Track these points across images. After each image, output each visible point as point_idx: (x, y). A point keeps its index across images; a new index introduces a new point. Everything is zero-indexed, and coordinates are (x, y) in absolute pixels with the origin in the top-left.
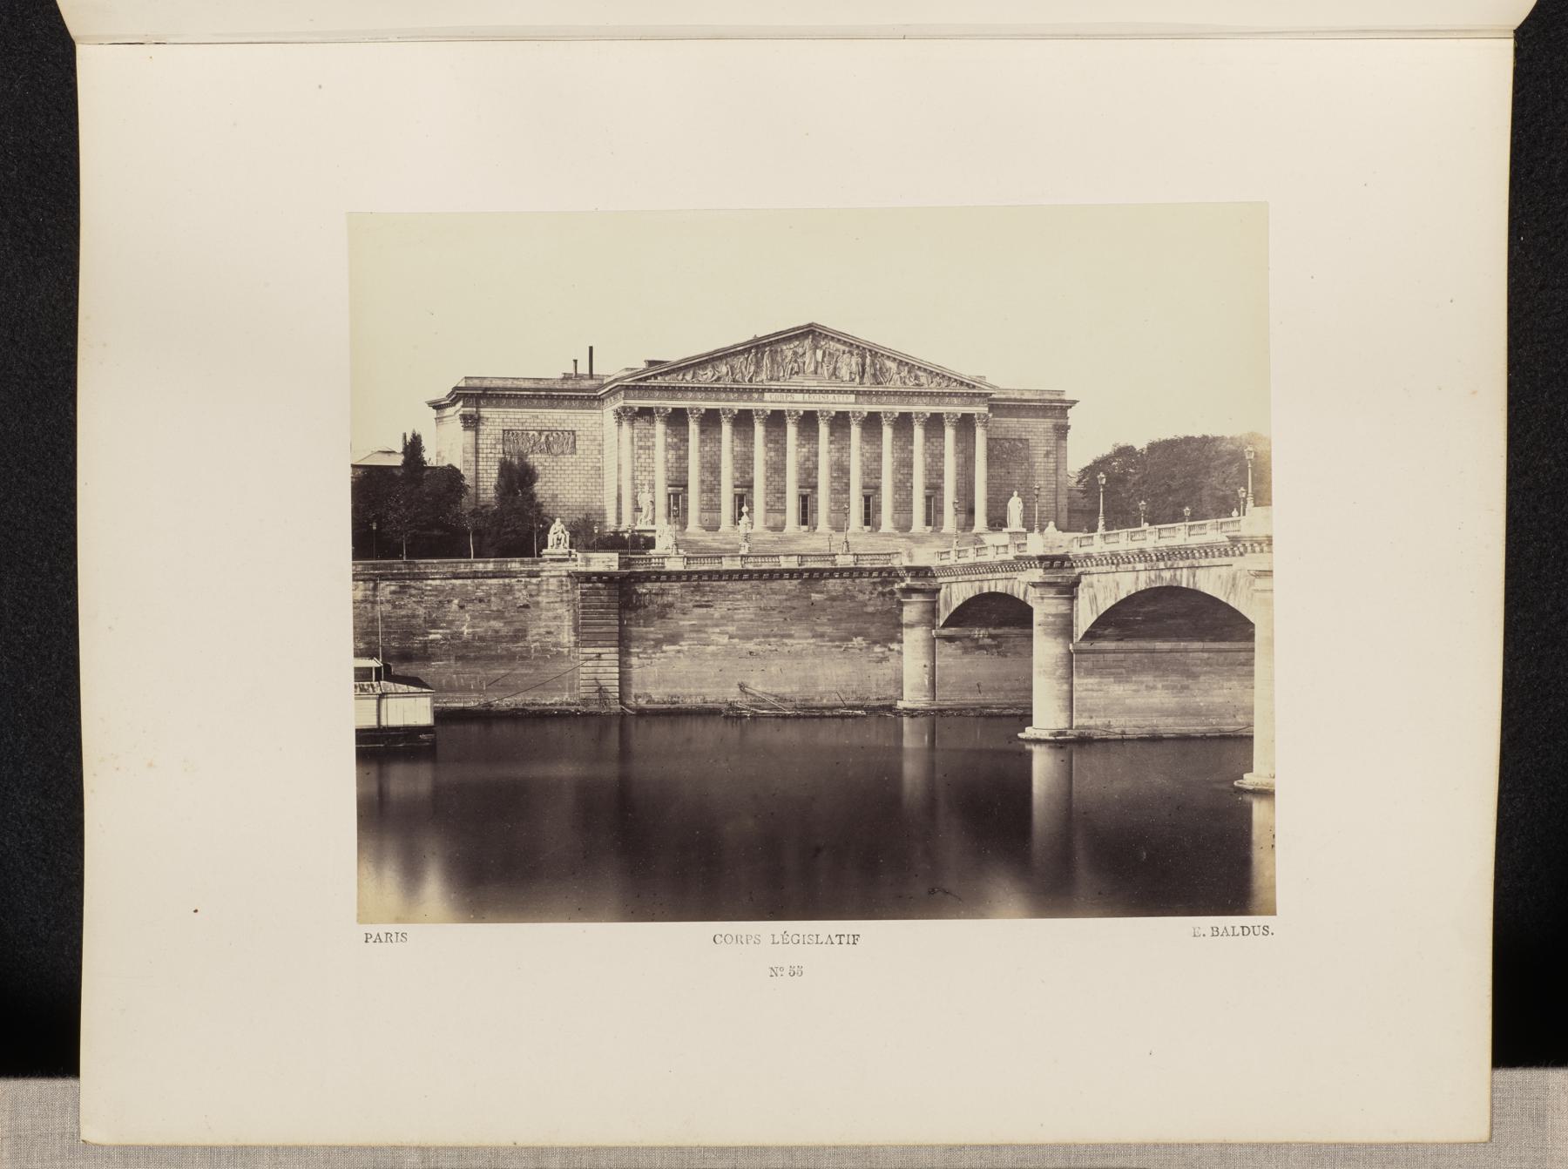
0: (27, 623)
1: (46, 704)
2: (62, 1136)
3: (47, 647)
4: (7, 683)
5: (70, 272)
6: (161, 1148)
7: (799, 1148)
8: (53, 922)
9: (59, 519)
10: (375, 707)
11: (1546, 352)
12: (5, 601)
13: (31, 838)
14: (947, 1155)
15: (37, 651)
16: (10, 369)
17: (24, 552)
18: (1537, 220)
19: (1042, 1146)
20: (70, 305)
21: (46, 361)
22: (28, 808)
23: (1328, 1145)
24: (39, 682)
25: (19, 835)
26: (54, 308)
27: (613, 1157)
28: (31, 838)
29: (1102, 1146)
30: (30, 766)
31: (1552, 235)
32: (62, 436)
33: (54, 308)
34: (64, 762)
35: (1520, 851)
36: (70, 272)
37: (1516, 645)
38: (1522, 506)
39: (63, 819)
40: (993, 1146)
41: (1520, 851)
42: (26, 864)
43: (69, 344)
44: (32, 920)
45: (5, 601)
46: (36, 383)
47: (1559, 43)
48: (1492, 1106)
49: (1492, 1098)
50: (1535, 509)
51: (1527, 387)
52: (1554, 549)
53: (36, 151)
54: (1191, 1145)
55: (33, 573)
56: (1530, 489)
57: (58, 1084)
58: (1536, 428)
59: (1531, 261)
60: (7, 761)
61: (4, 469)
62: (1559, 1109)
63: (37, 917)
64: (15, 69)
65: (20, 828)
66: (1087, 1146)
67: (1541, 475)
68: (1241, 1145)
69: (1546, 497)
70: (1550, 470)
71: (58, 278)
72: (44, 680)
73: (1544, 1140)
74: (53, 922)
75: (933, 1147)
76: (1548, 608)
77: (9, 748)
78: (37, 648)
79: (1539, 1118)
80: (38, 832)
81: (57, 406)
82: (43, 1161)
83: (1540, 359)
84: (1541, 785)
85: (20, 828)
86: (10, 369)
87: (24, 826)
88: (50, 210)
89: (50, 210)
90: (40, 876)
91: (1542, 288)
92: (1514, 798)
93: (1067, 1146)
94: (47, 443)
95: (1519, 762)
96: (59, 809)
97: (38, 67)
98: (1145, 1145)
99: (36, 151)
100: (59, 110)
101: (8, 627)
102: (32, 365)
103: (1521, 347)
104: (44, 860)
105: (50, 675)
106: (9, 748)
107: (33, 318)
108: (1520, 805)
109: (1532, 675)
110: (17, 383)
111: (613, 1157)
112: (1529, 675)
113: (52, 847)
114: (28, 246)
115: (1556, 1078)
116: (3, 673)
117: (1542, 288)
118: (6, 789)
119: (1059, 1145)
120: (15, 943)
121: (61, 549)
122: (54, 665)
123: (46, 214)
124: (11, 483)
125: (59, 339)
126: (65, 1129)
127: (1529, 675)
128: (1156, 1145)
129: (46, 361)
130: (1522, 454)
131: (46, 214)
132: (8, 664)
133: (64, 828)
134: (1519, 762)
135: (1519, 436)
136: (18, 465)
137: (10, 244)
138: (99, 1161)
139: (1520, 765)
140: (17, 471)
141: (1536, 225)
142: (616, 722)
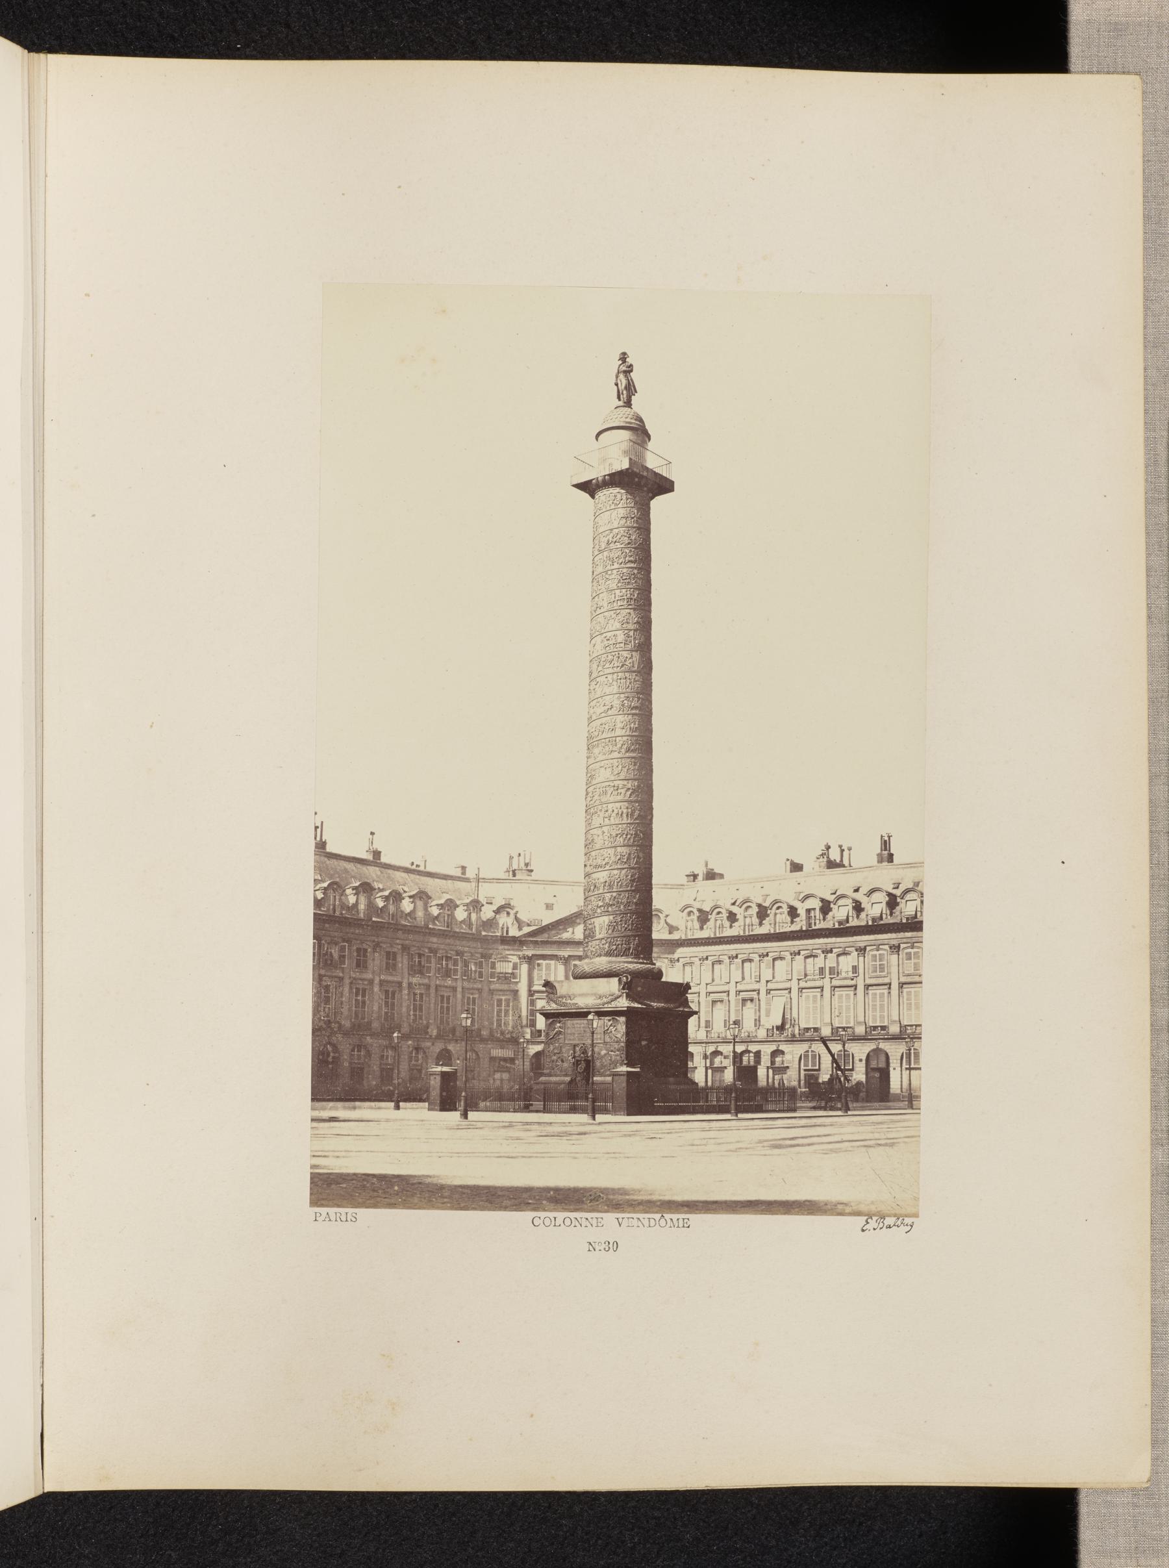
0: (623, 1542)
3: (648, 1521)
9: (519, 1510)
11: (352, 22)
12: (602, 1563)
13: (838, 1537)
15: (652, 1532)
17: (553, 1544)
20: (305, 1498)
22: (809, 1541)
23: (1145, 240)
30: (766, 1538)
31: (235, 15)
32: (436, 1506)
34: (762, 1503)
35: (852, 48)
39: (819, 1506)
41: (852, 48)
42: (864, 1542)
44: (920, 1536)
45: (602, 1563)
46: (383, 1532)
50: (509, 33)
51: (387, 41)
52: (549, 13)
54: (1146, 377)
55: (573, 1535)
56: (489, 38)
59: (261, 37)
60: (761, 1561)
61: (470, 1565)
64: (69, 1554)
66: (1146, 480)
68: (1145, 327)
70: (470, 18)
71: (279, 1510)
73: (1140, 24)
76: (608, 20)
77: (748, 1559)
79: (1118, 29)
80: (832, 1530)
82: (1161, 1525)
83: (359, 28)
84: (785, 27)
87: (826, 1544)
88: (210, 1518)
89: (210, 1518)
90: (877, 1528)
91: (288, 26)
93: (1148, 502)
94: (444, 1521)
95: (762, 49)
96: (809, 1509)
99: (152, 1532)
100: (111, 1508)
103: (348, 47)
104: (861, 1524)
105: (675, 1519)
107: (319, 1535)
108: (806, 49)
109: (676, 36)
114: (246, 1540)
116: (674, 1565)
117: (288, 26)
118: (789, 1562)
120: (944, 1553)
121: (549, 1507)
122: (665, 1514)
123: (214, 1522)
124: (484, 1557)
125: (340, 1509)
127: (675, 39)
128: (1146, 411)
130: (454, 46)
131: (214, 1522)
134: (762, 49)
135: (436, 49)
136: (465, 1550)
137: (245, 1558)
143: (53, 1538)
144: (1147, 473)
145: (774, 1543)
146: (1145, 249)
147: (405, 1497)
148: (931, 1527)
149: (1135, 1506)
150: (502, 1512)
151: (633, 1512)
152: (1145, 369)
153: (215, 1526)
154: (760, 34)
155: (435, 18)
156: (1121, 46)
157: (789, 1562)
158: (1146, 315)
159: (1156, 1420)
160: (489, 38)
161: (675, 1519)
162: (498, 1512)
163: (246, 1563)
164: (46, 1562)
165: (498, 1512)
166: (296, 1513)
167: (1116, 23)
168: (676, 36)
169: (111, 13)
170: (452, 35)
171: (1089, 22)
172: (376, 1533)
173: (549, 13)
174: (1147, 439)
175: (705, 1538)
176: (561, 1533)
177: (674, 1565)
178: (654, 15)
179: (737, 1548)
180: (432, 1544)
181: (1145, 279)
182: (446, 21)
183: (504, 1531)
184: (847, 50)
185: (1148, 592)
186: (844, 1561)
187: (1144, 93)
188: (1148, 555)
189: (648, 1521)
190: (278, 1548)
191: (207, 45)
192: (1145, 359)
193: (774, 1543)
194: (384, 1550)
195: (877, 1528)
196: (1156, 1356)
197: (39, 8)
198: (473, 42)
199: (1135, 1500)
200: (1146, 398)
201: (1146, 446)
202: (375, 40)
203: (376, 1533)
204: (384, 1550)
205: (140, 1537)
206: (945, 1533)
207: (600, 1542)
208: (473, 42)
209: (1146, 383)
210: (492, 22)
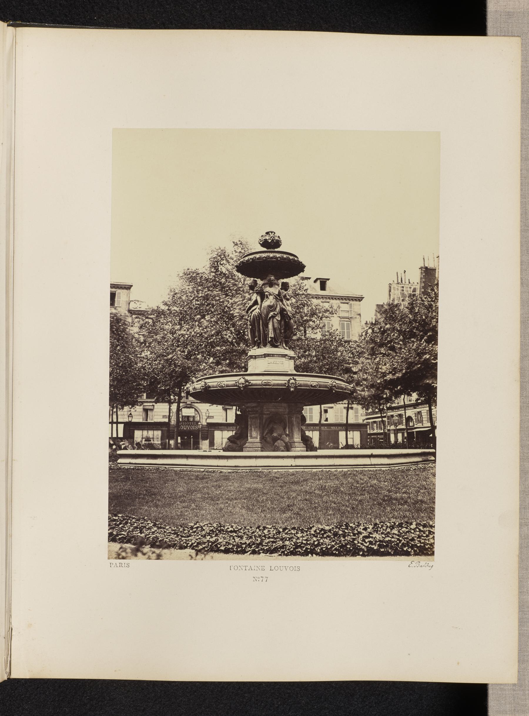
0: (273, 704)
1: (311, 695)
2: (514, 690)
3: (285, 695)
4: (301, 713)
5: (112, 684)
6: (520, 645)
7: (521, 353)
8: (411, 692)
9: (225, 689)
10: (119, 419)
11: (148, 7)
12: (264, 714)
13: (372, 702)
14: (525, 286)
15: (286, 700)
16: (157, 712)
17: (241, 705)
18: (87, 12)
19: (521, 242)
20: (127, 684)
21: (153, 695)
22: (359, 704)
23: (522, 111)
24: (300, 698)
25: (371, 707)
26: (129, 691)
27: (525, 439)
28: (372, 702)
29: (521, 215)
30: (339, 703)
31: (94, 4)
32: (187, 688)
33: (129, 691)
34: (337, 686)
35: (378, 19)
36: (112, 684)
37: (283, 21)
38: (219, 17)
39: (363, 688)
40: (521, 265)
41: (378, 19)
42: (384, 704)
43: (145, 685)
44: (410, 701)
45: (264, 714)
46: (163, 700)
47: (6, 3)
48: (504, 36)
49: (500, 36)
50: (220, 12)
51: (164, 15)
52: (239, 3)
53: (57, 699)
54: (521, 174)
55: (250, 701)
56: (211, 14)
57: (490, 692)
58: (183, 11)
59: (106, 14)
60: (337, 713)
61: (203, 715)
62: (506, 6)
63: (409, 700)
64: (18, 708)
65: (368, 707)
66: (521, 221)
67: (204, 9)
68: (521, 151)
69: (214, 7)
70: (202, 5)
71: (115, 690)
72: (300, 696)
73: (519, 13)
74: (411, 692)
75: (521, 292)
76: (265, 6)
77: (331, 712)
78: (285, 699)
79: (509, 15)
80: (370, 699)
81: (173, 690)
82: (526, 699)
83: (151, 9)
84: (347, 9)
85: (368, 707)
86: (157, 712)
87: (367, 705)
88: (83, 693)
89: (83, 693)
90: (390, 698)
91: (118, 9)
92: (353, 21)
93: (521, 231)
94: (191, 695)
95: (336, 19)
96: (359, 689)
97: (17, 697)
98: (521, 195)
99: (57, 699)
100: (38, 688)
101: (275, 712)
102: (155, 701)
103: (146, 18)
104: (383, 696)
105: (297, 693)
106: (331, 712)
107: (133, 701)
108: (356, 19)
109: (297, 13)
110: (163, 708)
111: (525, 439)
112: (296, 14)
113: (376, 692)
114: (100, 703)
115: (492, 6)
116: (297, 715)
117: (118, 9)
118: (350, 713)
119: (521, 234)
120: (421, 709)
121: (239, 688)
122: (293, 692)
123: (85, 695)
124: (209, 711)
125: (143, 689)
126: (511, 689)
127: (296, 14)
128: (521, 190)
129: (153, 695)
130: (195, 18)
131: (85, 695)
132: (292, 712)
133: (368, 687)
134: (336, 19)
135: (186, 19)
136: (201, 708)
137: (99, 712)
138: (526, 674)
139: (338, 18)
140: (203, 708)
141: (89, 12)
142: (336, 445)
143: (10, 701)
144: (521, 218)
145: (343, 704)
146: (522, 115)
147: (173, 684)
148: (415, 697)
149: (514, 690)
150: (217, 691)
151: (278, 691)
152: (521, 170)
153: (86, 697)
154: (335, 12)
155: (186, 5)
156: (511, 22)
157: (350, 713)
158: (522, 146)
159: (521, 651)
160: (211, 14)
161: (297, 693)
162: (216, 691)
163: (100, 714)
164: (7, 712)
165: (216, 691)
166: (123, 691)
167: (509, 12)
168: (297, 13)
169: (38, 5)
170: (194, 13)
171: (496, 11)
172: (160, 700)
173: (239, 3)
174: (521, 202)
175: (311, 702)
176: (245, 700)
177: (297, 715)
178: (286, 4)
179: (326, 707)
180: (186, 705)
181: (521, 129)
182: (191, 6)
183: (218, 699)
184: (376, 19)
185: (521, 272)
186: (375, 713)
187: (522, 44)
188: (522, 256)
189: (285, 695)
190: (115, 707)
191: (81, 18)
192: (521, 166)
193: (343, 704)
194: (163, 708)
195: (390, 698)
196: (522, 622)
197: (4, 2)
198: (204, 16)
199: (514, 688)
200: (521, 184)
201: (521, 205)
202: (158, 15)
203: (160, 700)
204: (163, 708)
205: (52, 702)
206: (421, 700)
207: (263, 704)
208: (204, 16)
209: (521, 177)
210: (212, 6)
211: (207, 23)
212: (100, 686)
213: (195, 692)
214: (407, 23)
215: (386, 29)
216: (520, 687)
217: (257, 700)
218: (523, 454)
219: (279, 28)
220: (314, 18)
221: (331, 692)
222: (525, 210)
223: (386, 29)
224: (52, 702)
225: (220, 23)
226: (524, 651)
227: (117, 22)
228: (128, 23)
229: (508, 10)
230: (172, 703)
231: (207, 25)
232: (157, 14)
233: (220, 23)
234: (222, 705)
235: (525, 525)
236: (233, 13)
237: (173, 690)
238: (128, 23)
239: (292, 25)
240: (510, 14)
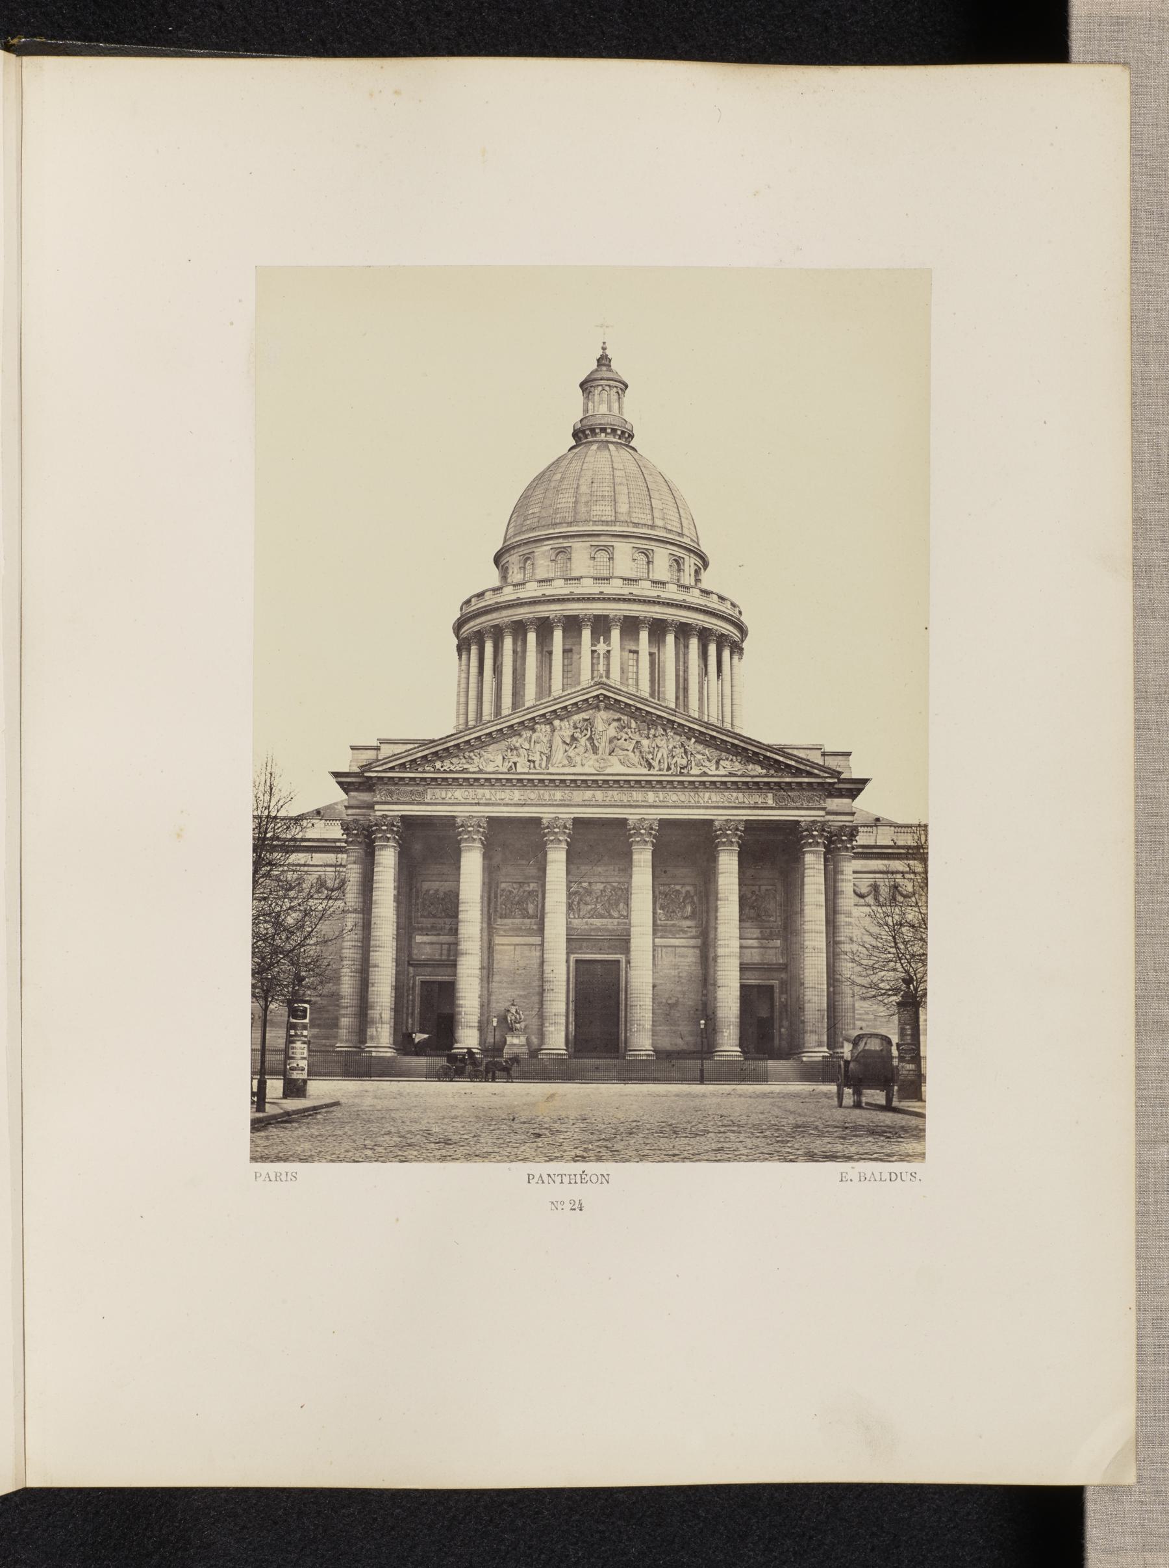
1: (650, 1535)
3: (592, 1536)
8: (875, 1529)
9: (460, 1523)
15: (596, 1546)
17: (495, 1558)
18: (152, 15)
22: (757, 1555)
26: (244, 1527)
27: (1162, 952)
30: (714, 1552)
33: (244, 1527)
34: (710, 1516)
39: (768, 1519)
42: (814, 1557)
44: (872, 1550)
46: (320, 1547)
50: (448, 14)
51: (323, 22)
55: (515, 1549)
59: (194, 19)
67: (414, 8)
71: (213, 1524)
73: (1141, 19)
74: (875, 1529)
78: (592, 1545)
79: (1119, 23)
80: (782, 1544)
81: (344, 1525)
87: (776, 1558)
96: (758, 1522)
100: (49, 1515)
102: (302, 1550)
104: (811, 1538)
109: (619, 17)
111: (1162, 952)
121: (491, 1521)
125: (276, 1523)
129: (298, 1536)
130: (393, 28)
135: (373, 31)
141: (156, 16)
145: (722, 1557)
148: (884, 1541)
149: (1142, 1503)
150: (442, 1526)
156: (1123, 40)
160: (428, 19)
162: (438, 1526)
165: (438, 1526)
166: (231, 1527)
167: (1118, 18)
168: (619, 17)
170: (390, 17)
171: (1090, 17)
175: (651, 1552)
183: (444, 1545)
189: (592, 1536)
190: (212, 1562)
193: (722, 1557)
195: (827, 1542)
199: (1142, 1498)
211: (419, 40)
212: (179, 1516)
213: (393, 1528)
214: (866, 40)
215: (819, 52)
216: (1155, 1496)
217: (530, 1547)
218: (1158, 987)
219: (604, 54)
220: (658, 28)
221: (696, 1528)
222: (1157, 450)
223: (819, 52)
224: (80, 1545)
225: (449, 39)
226: (1163, 1417)
227: (218, 38)
228: (244, 40)
229: (1115, 14)
230: (341, 1555)
231: (420, 44)
232: (308, 21)
233: (449, 39)
234: (452, 1559)
235: (1163, 1140)
236: (477, 18)
237: (344, 1525)
238: (244, 40)
239: (609, 45)
240: (1121, 21)
